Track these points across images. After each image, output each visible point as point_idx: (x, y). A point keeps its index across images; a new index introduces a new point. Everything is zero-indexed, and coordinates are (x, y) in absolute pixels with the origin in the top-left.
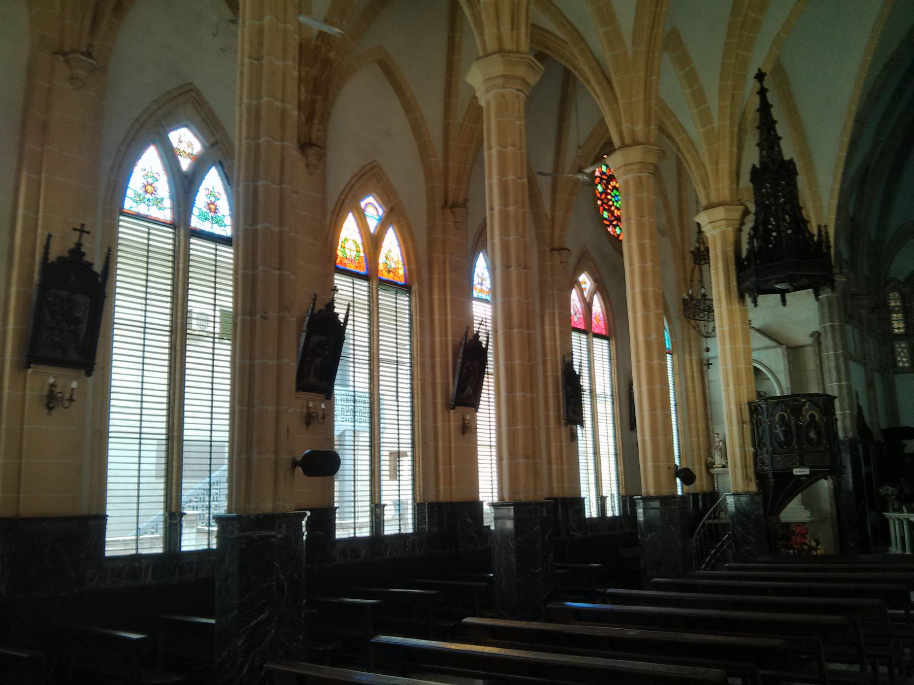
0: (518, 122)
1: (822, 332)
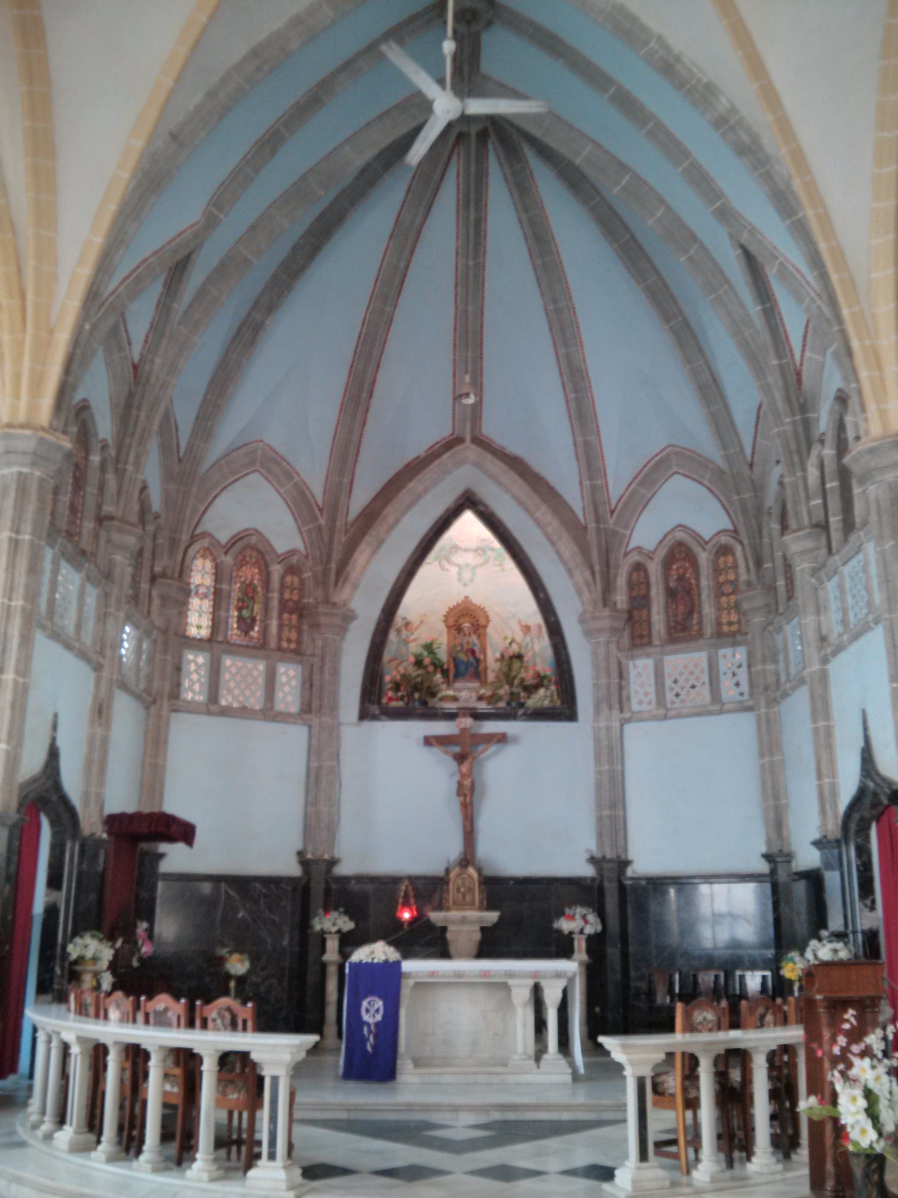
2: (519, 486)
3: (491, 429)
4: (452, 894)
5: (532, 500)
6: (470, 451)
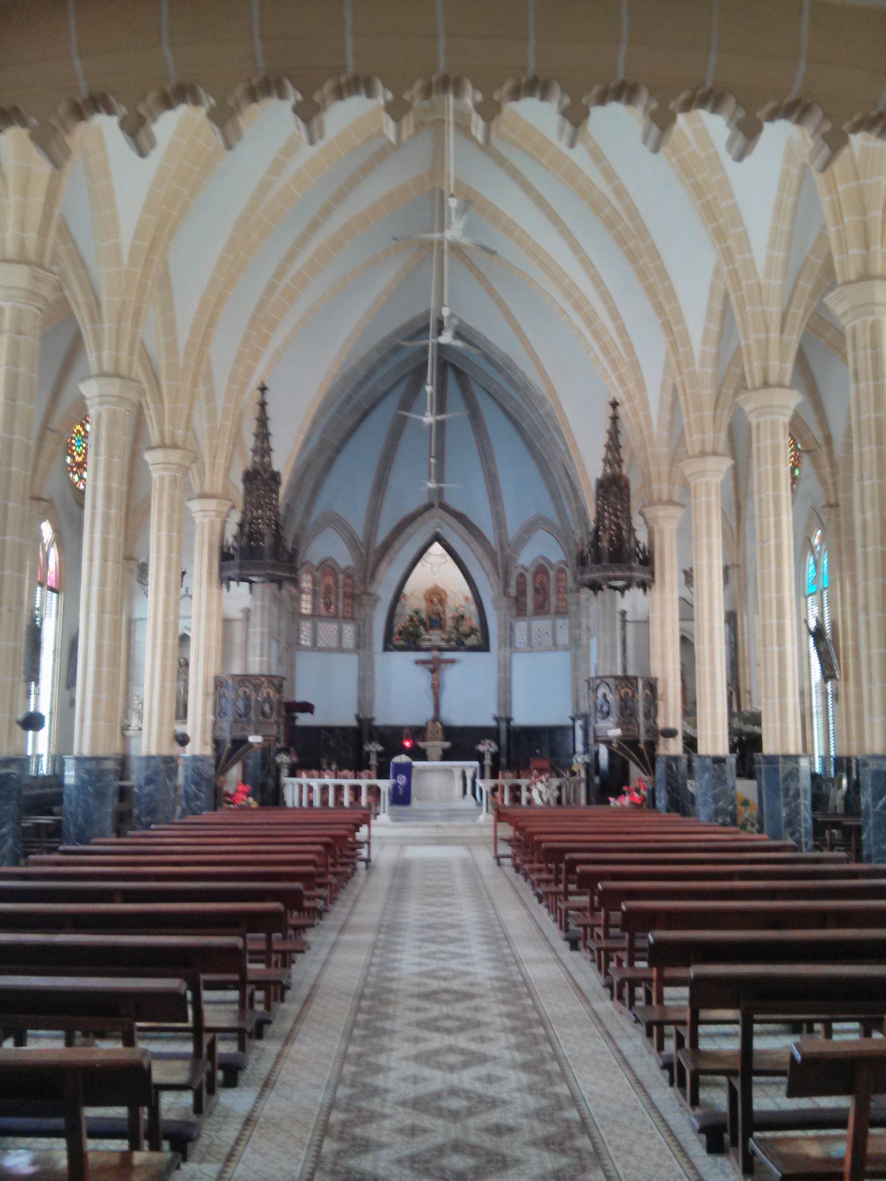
0: (123, 437)
1: (252, 609)
3: (450, 500)
4: (429, 734)
5: (470, 538)
6: (437, 512)
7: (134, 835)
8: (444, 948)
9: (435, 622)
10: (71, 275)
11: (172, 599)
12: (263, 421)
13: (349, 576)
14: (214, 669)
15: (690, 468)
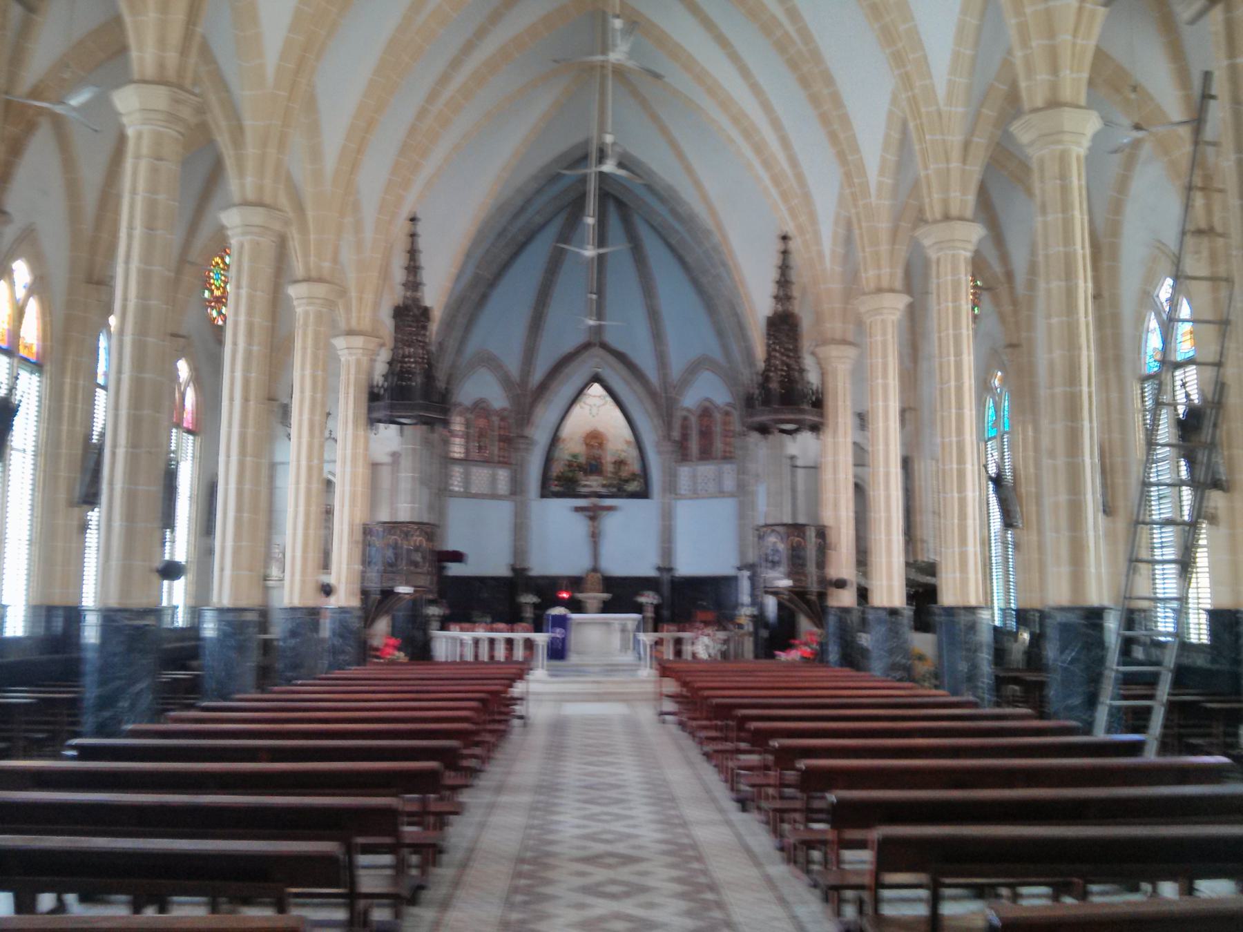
2: (624, 371)
3: (611, 339)
7: (279, 691)
8: (605, 809)
9: (594, 467)
10: (213, 99)
11: (316, 441)
12: (413, 253)
13: (503, 419)
14: (360, 517)
15: (865, 305)
